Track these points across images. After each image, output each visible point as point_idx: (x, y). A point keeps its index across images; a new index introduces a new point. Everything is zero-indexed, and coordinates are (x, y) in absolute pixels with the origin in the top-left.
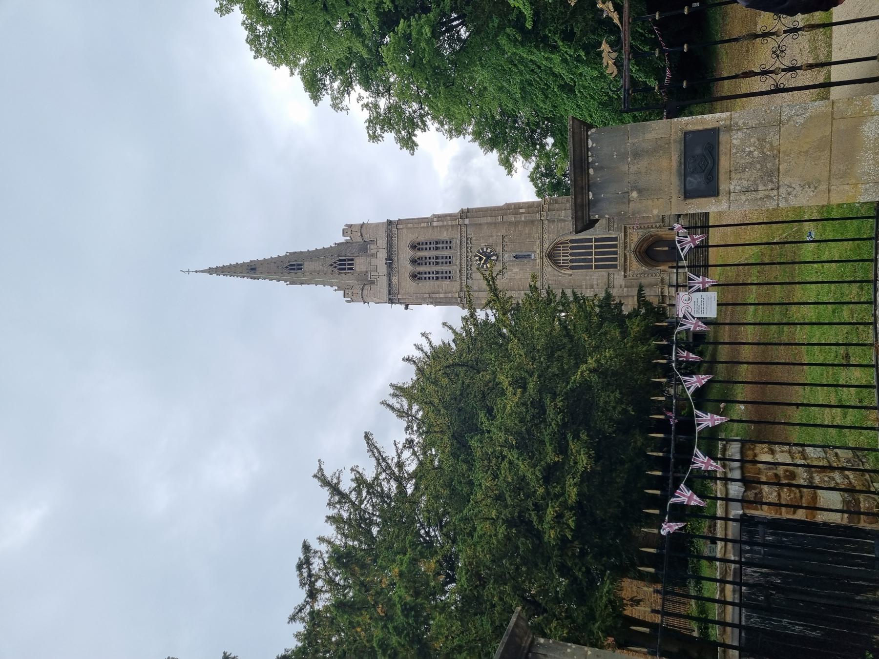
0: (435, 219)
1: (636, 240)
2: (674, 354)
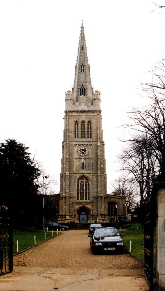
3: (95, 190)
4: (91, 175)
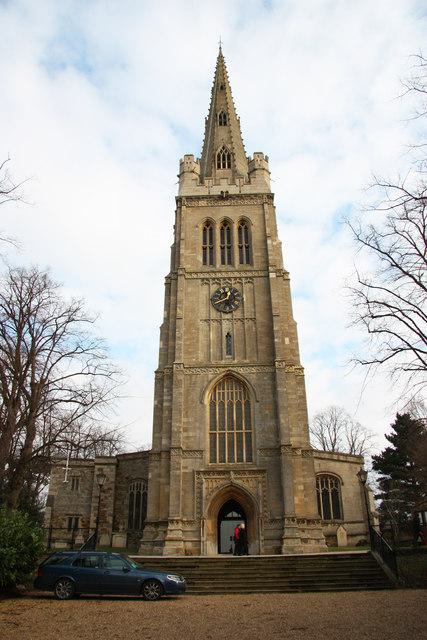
0: (274, 243)
1: (246, 485)
2: (64, 566)
3: (272, 423)
4: (254, 370)
